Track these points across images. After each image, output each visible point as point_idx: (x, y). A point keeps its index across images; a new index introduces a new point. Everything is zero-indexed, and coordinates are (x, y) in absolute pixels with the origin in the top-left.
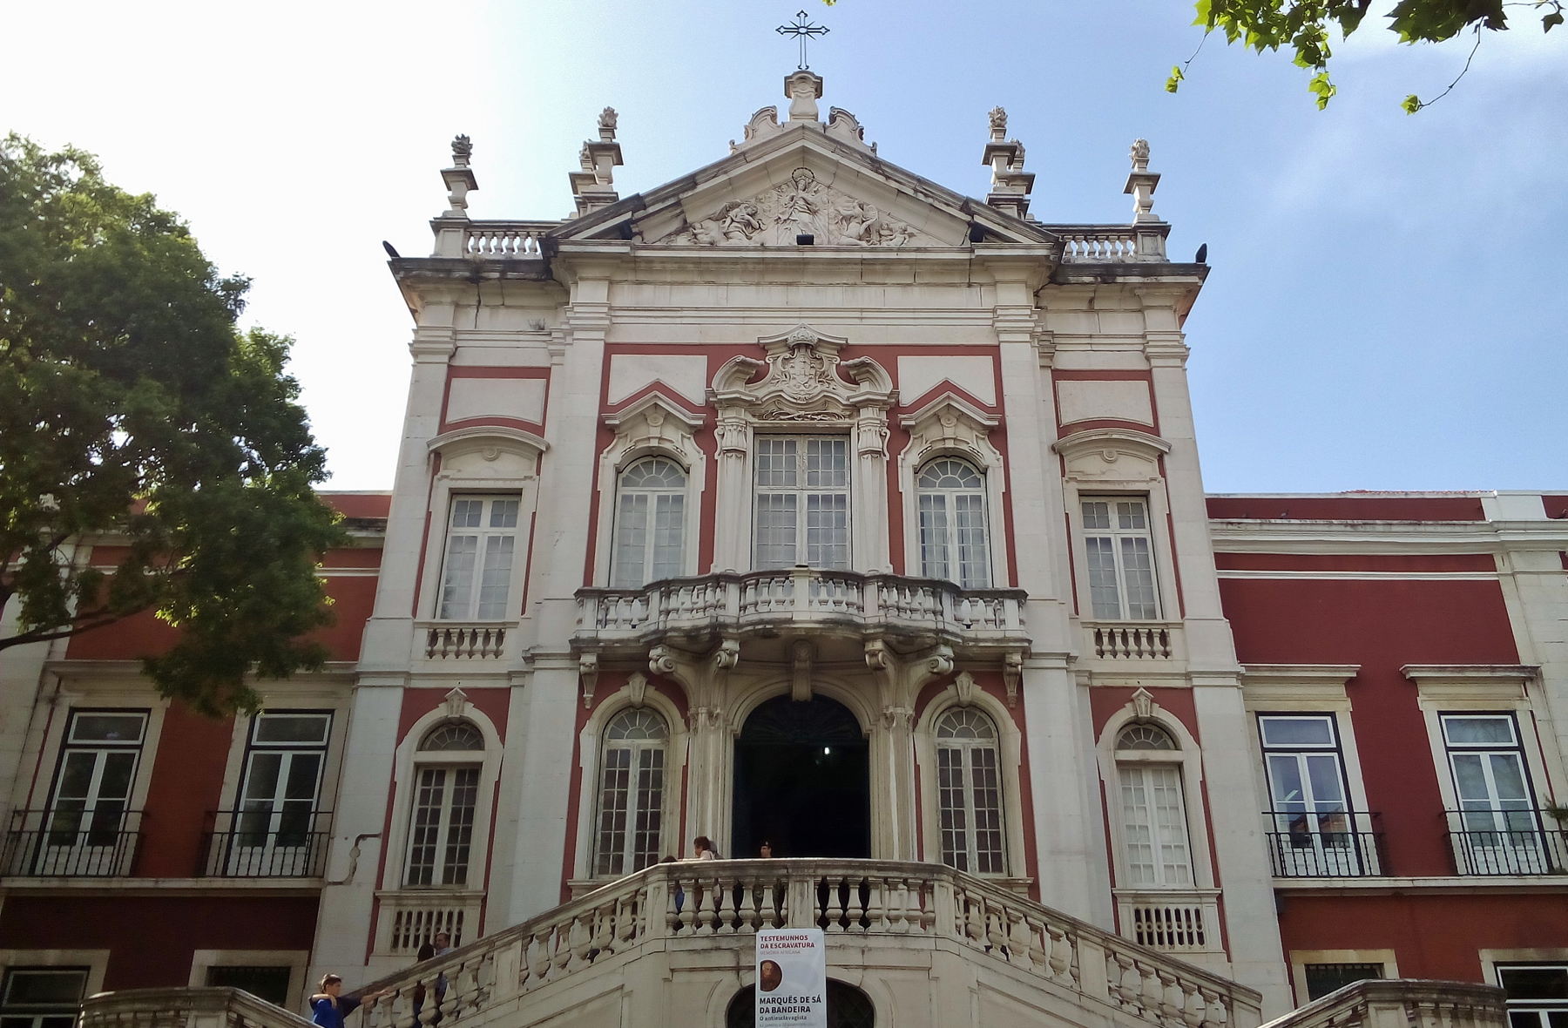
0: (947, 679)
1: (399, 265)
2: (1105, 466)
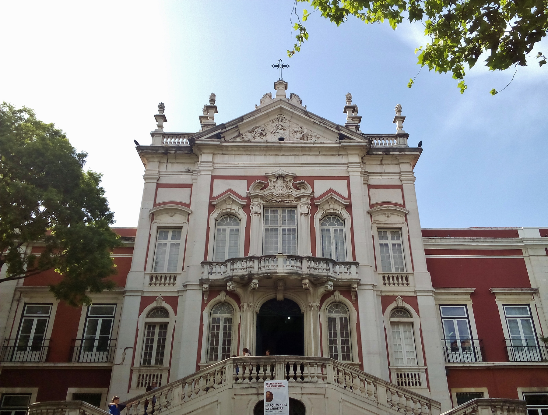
0: (331, 293)
1: (139, 148)
2: (386, 218)
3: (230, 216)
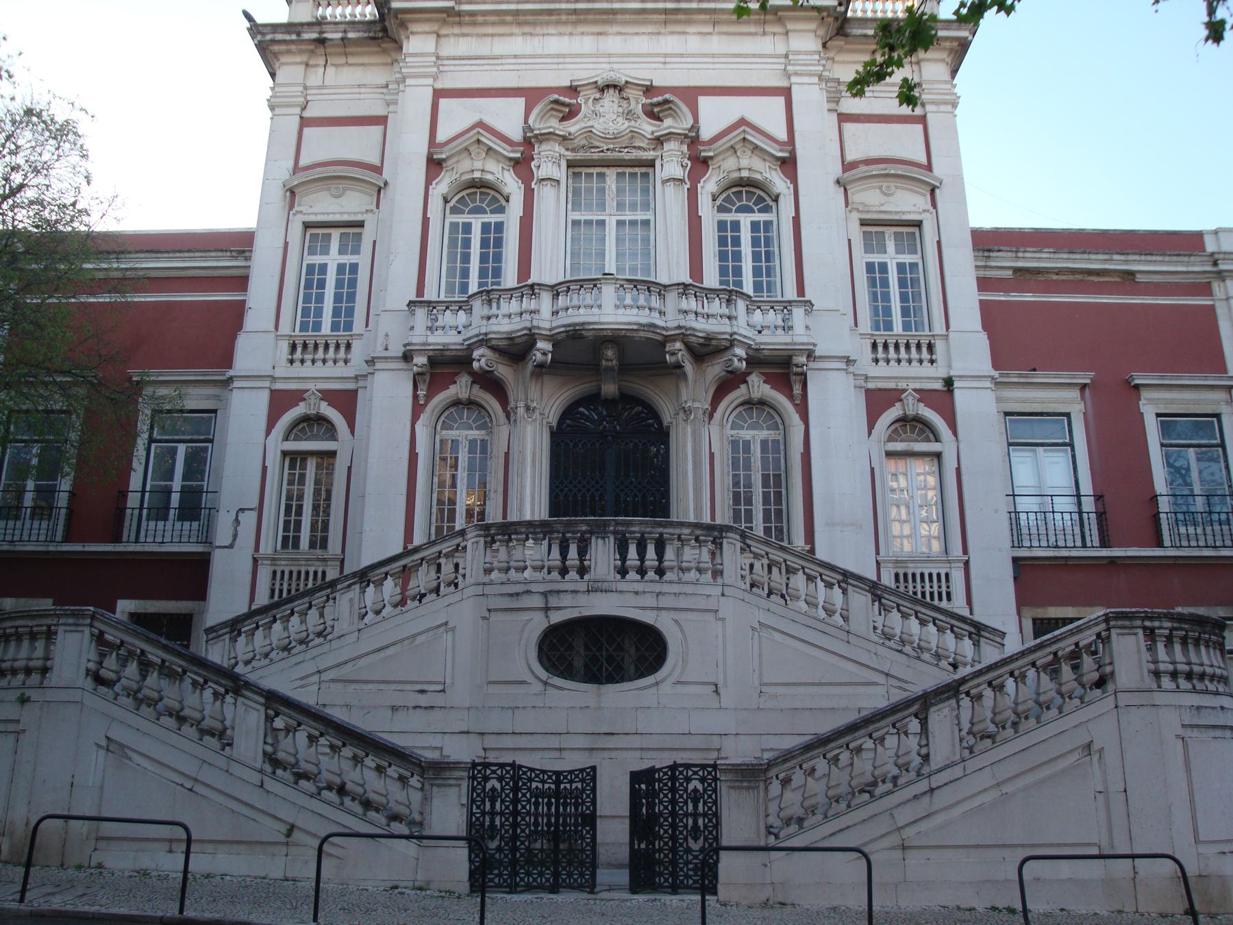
1: (256, 29)
2: (883, 199)
3: (482, 190)
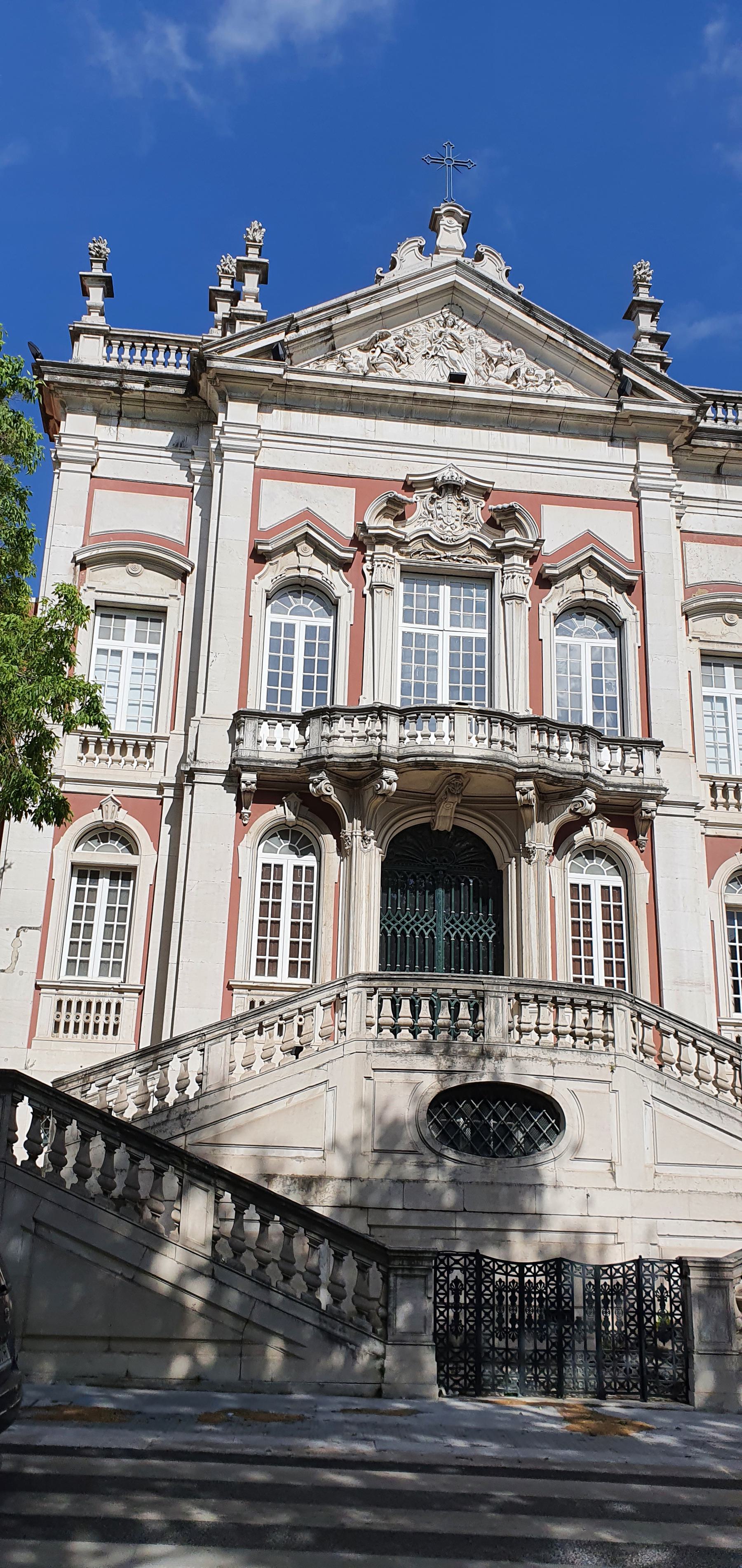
0: (584, 820)
